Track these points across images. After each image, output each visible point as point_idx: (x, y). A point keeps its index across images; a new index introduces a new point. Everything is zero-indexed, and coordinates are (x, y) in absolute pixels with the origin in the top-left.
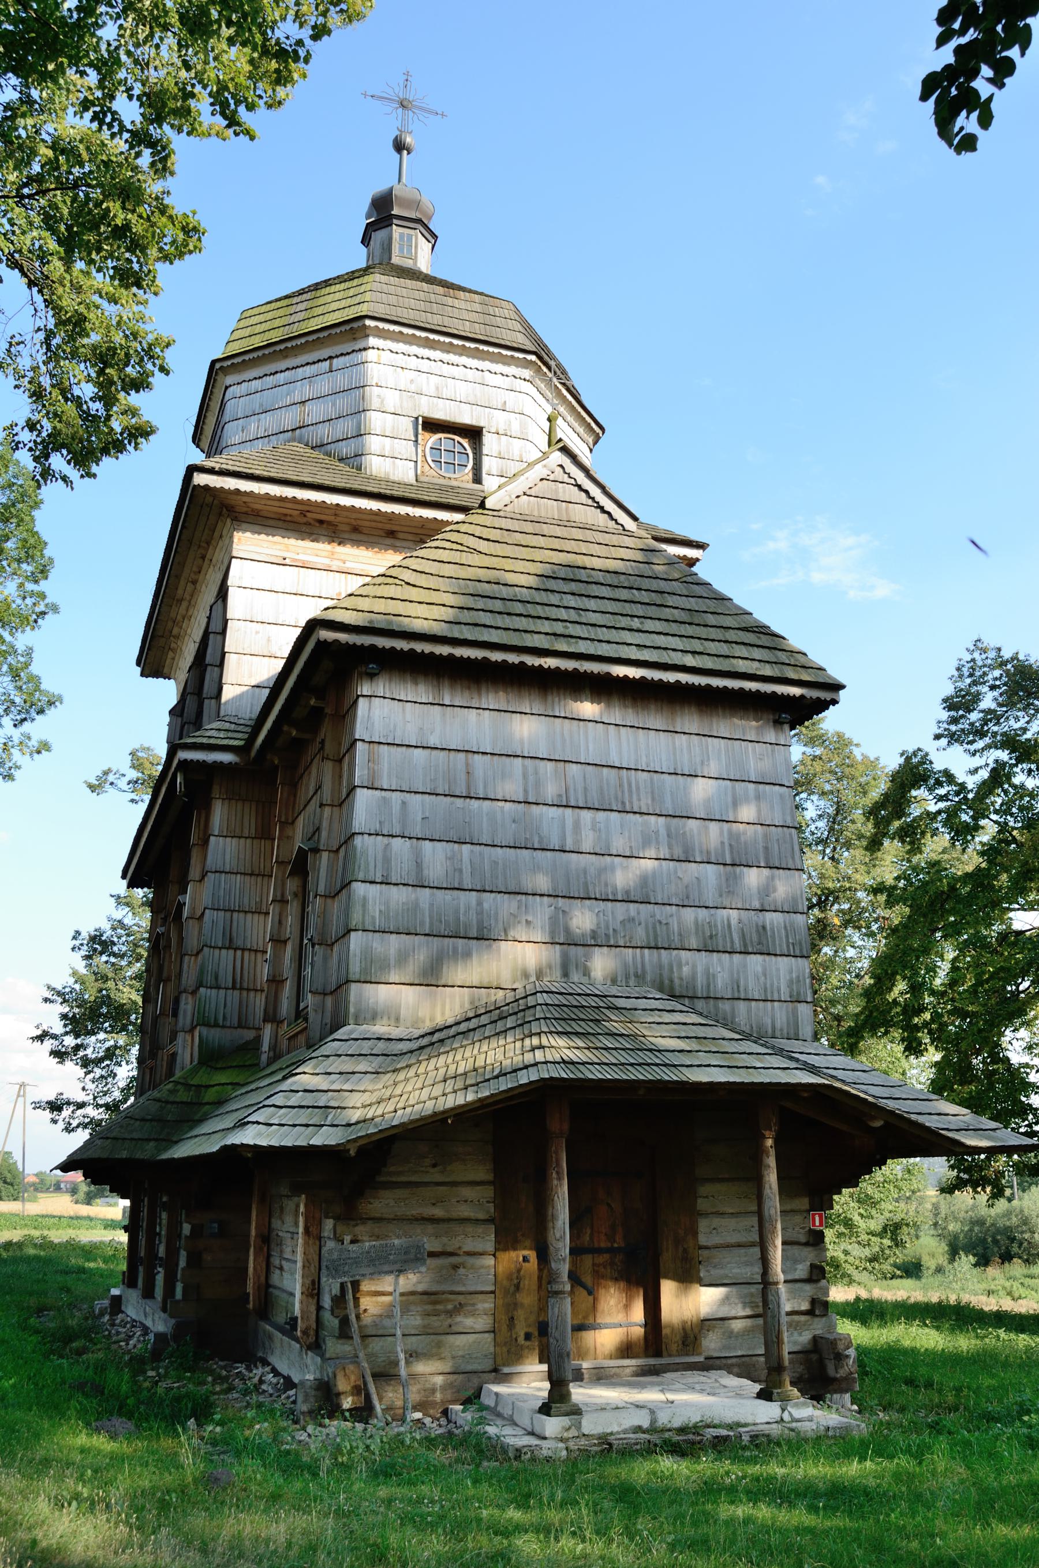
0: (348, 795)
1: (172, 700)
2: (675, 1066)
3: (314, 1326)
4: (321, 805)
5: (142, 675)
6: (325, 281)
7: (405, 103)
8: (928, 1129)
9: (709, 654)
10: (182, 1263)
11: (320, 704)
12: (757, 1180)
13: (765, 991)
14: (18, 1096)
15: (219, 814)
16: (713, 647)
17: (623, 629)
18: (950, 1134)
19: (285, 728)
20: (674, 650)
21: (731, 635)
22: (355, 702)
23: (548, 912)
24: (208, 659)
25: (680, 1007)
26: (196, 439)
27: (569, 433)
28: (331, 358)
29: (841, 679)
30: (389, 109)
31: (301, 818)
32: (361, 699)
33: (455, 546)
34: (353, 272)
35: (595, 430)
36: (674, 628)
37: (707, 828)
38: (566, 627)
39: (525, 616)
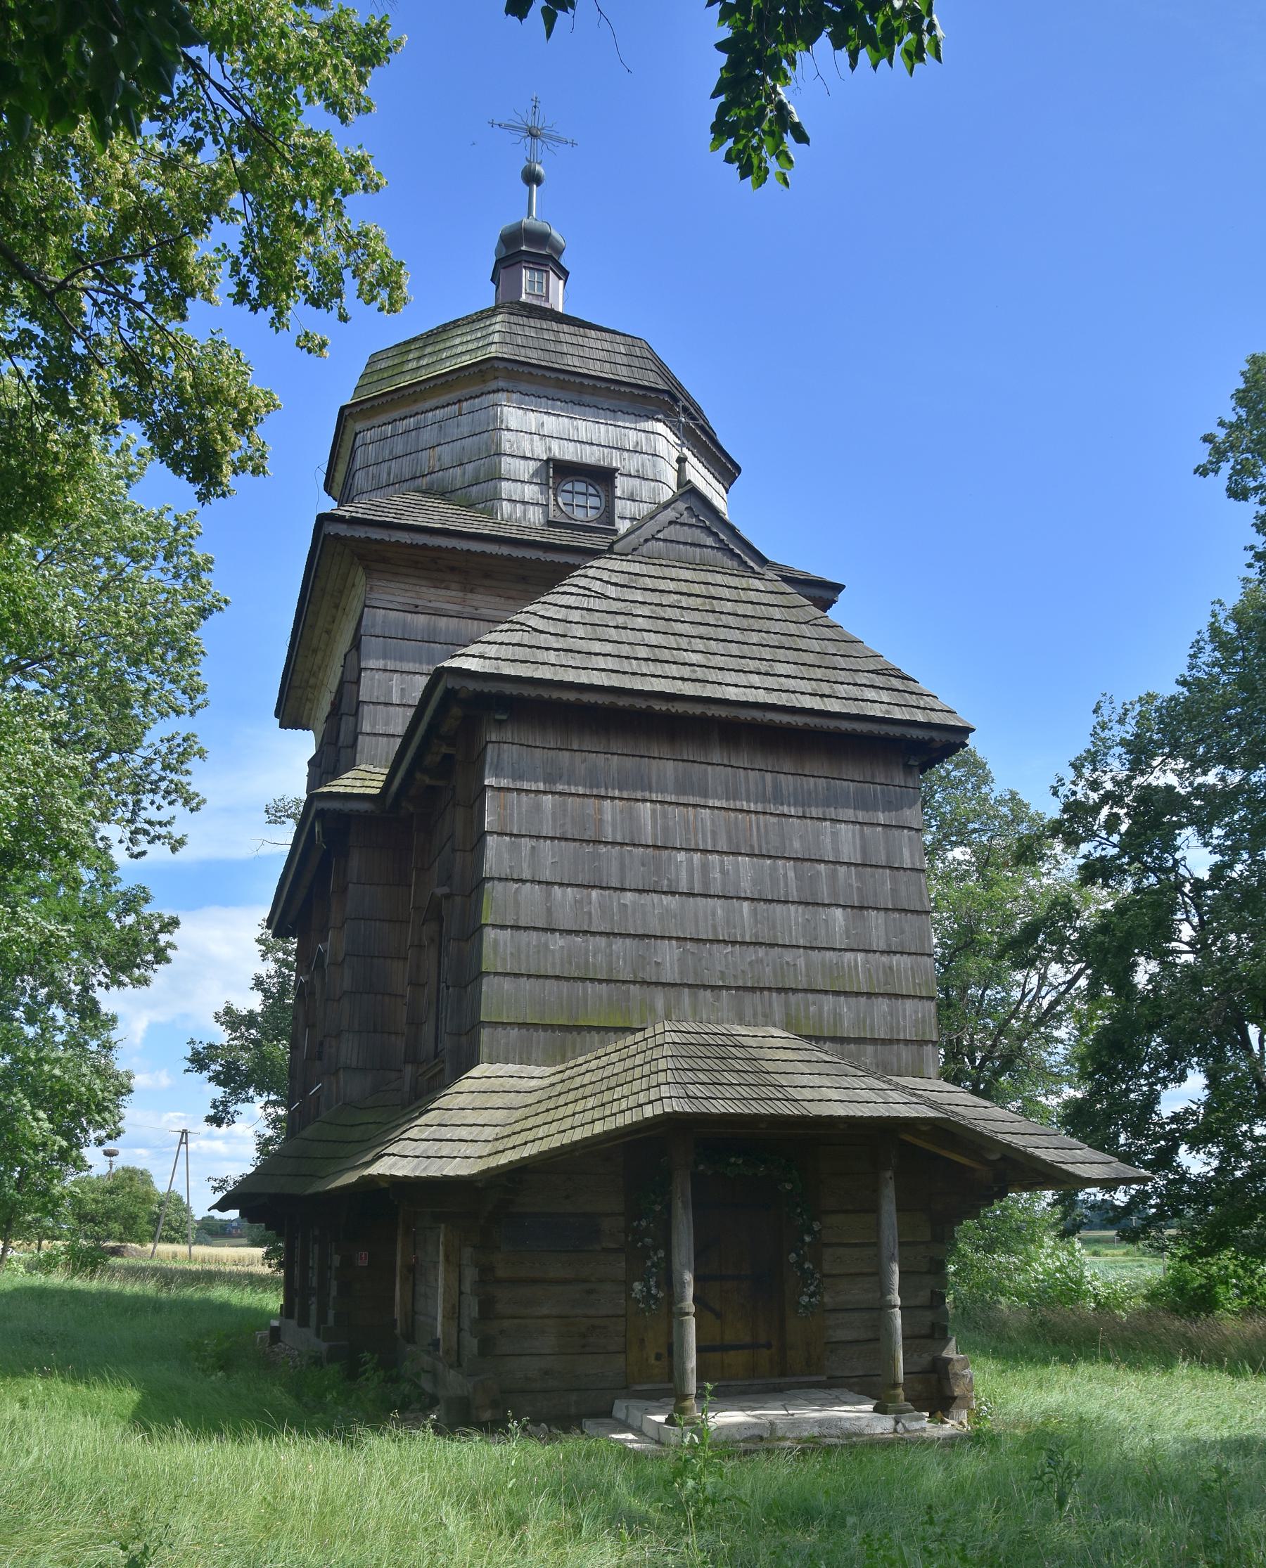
0: (479, 841)
1: (311, 751)
2: (796, 1100)
3: (456, 1347)
4: (454, 850)
5: (281, 727)
6: (454, 322)
7: (534, 132)
8: (1044, 1161)
9: (837, 698)
10: (334, 1292)
11: (451, 751)
12: (875, 1209)
13: (892, 1029)
14: (181, 1143)
15: (355, 862)
16: (841, 690)
17: (751, 672)
18: (1064, 1167)
19: (418, 775)
20: (802, 693)
21: (862, 678)
22: (485, 749)
23: (677, 952)
24: (344, 709)
25: (808, 1046)
26: (328, 487)
27: (699, 475)
28: (460, 401)
29: (970, 722)
30: (517, 139)
31: (436, 864)
32: (490, 746)
33: (581, 591)
34: (481, 312)
35: (727, 470)
36: (806, 672)
37: (835, 871)
38: (695, 671)
39: (653, 661)
